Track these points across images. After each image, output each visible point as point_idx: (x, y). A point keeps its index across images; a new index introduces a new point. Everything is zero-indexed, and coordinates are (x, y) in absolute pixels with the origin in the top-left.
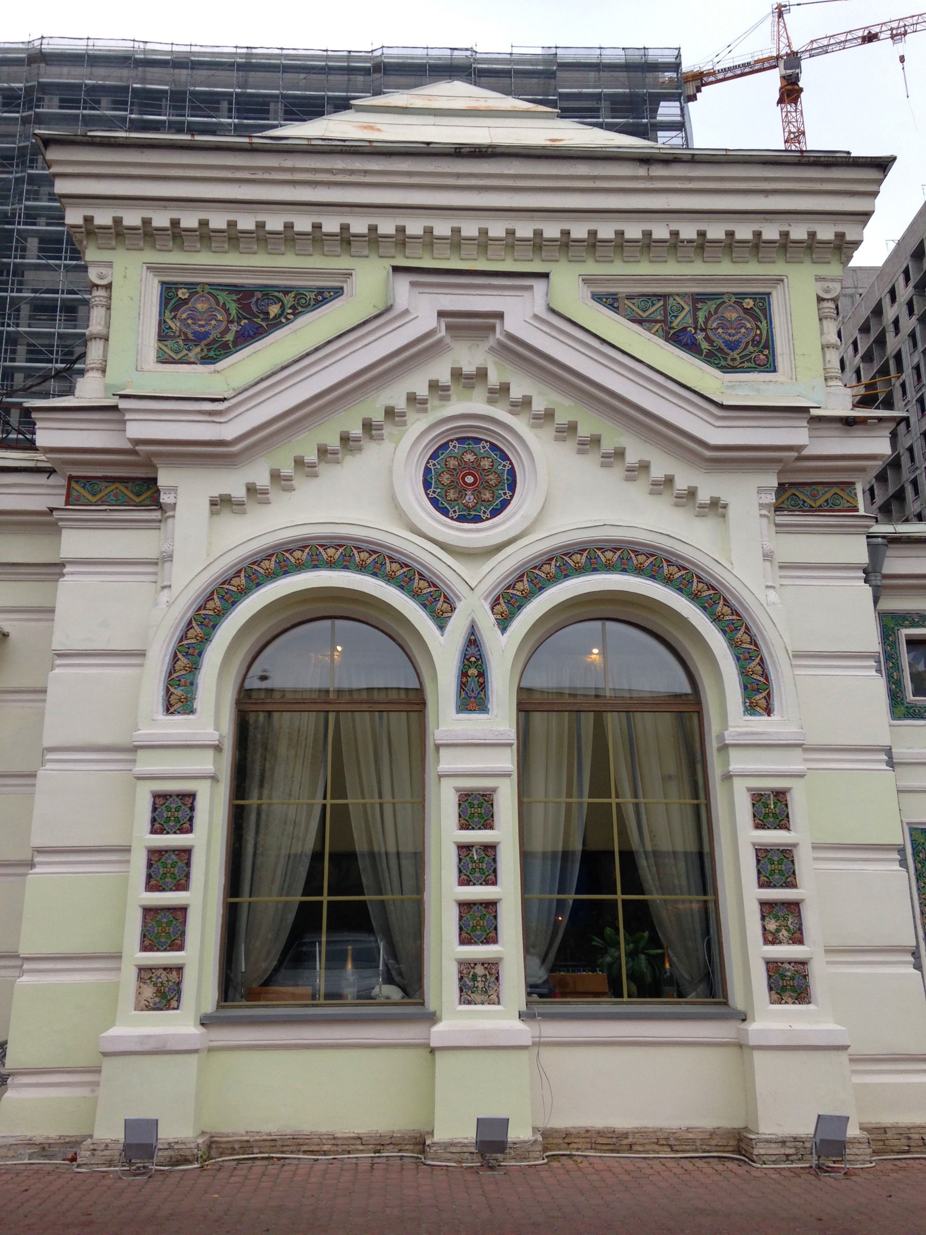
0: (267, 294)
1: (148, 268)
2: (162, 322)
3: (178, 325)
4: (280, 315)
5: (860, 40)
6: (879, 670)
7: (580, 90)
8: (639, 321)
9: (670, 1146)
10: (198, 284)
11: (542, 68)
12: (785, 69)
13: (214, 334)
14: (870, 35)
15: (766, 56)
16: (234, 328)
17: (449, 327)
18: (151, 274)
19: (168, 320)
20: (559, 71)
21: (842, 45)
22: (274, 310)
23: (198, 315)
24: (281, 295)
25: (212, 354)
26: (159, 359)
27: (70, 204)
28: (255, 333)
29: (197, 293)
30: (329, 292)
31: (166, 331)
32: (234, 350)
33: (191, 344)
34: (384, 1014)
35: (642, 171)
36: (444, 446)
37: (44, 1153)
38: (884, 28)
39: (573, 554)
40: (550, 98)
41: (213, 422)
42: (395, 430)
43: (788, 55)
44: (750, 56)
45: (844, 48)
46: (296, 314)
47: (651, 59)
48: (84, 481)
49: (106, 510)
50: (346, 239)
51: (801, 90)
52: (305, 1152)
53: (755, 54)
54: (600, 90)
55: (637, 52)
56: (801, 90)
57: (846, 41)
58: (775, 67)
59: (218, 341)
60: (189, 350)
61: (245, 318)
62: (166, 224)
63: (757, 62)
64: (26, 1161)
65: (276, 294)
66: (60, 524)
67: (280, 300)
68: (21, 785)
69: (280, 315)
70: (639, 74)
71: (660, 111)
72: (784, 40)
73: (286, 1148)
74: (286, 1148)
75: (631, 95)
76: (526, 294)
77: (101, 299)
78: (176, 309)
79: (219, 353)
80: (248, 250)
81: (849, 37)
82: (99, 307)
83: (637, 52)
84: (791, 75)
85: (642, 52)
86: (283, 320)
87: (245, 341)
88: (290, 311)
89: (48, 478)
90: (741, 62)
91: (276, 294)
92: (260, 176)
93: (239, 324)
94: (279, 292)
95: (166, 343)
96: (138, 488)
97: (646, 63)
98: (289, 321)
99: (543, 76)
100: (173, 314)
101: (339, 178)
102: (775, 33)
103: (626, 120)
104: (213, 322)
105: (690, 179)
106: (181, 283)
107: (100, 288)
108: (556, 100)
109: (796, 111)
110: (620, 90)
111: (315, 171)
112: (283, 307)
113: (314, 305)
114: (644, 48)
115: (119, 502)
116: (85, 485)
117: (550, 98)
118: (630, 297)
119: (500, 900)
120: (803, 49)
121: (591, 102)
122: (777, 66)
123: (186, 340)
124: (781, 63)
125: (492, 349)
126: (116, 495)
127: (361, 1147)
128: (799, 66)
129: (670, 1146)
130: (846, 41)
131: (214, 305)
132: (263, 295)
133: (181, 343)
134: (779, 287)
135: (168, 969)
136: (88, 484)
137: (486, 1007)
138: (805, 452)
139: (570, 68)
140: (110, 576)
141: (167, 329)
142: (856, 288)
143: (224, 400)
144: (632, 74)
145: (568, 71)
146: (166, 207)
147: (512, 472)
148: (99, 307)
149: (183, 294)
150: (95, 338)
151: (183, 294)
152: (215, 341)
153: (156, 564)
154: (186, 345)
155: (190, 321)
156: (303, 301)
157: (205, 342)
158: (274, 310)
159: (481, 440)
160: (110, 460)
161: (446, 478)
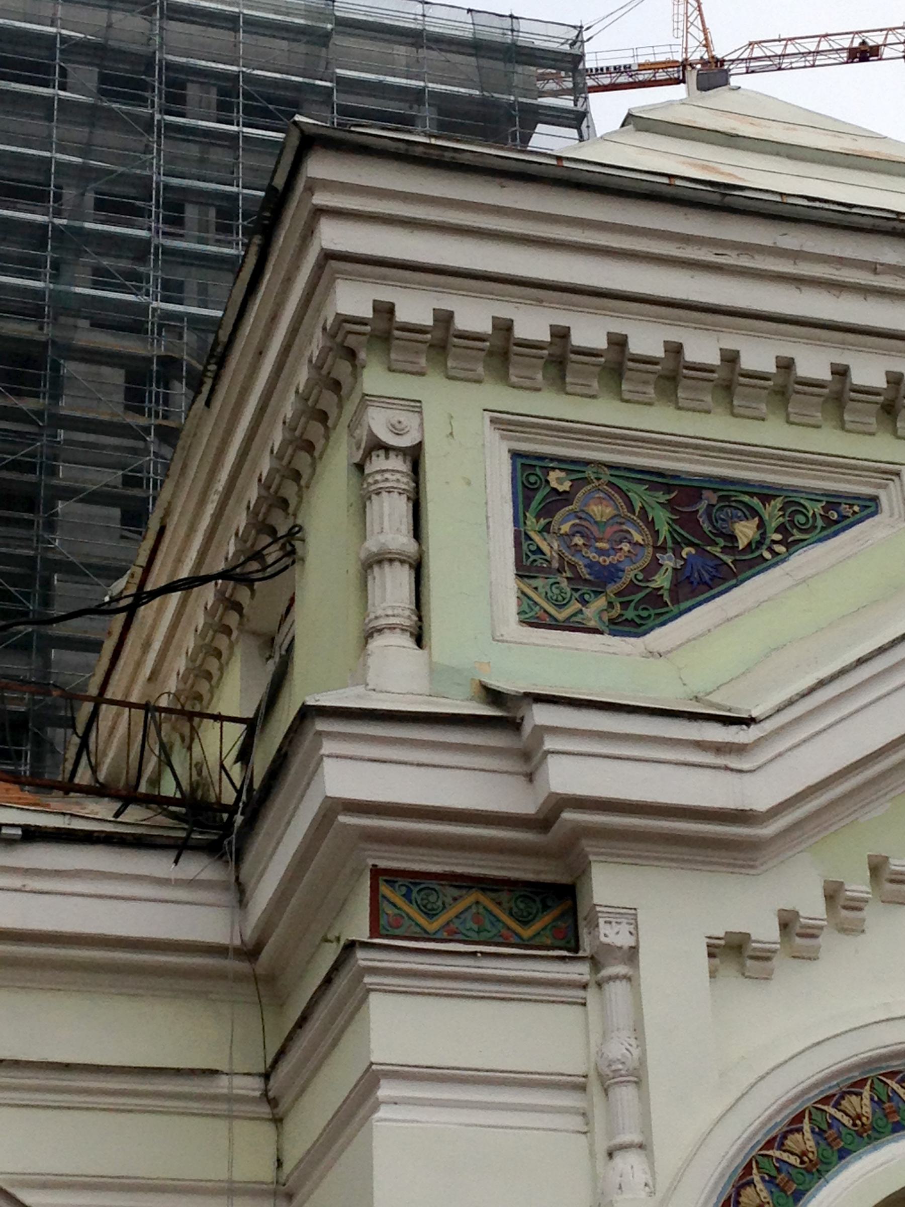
0: (729, 497)
1: (492, 421)
2: (521, 538)
3: (555, 545)
4: (760, 544)
5: (845, 55)
7: (381, 78)
10: (587, 463)
11: (302, 21)
13: (631, 572)
14: (863, 48)
15: (661, 58)
16: (669, 562)
18: (497, 434)
19: (532, 534)
20: (338, 33)
21: (810, 58)
22: (745, 531)
23: (594, 529)
24: (755, 502)
25: (630, 614)
26: (523, 617)
28: (713, 578)
29: (586, 481)
30: (851, 506)
31: (533, 557)
32: (675, 610)
33: (585, 589)
38: (891, 39)
39: (842, 1098)
40: (318, 82)
41: (727, 768)
43: (703, 62)
44: (630, 53)
45: (813, 66)
46: (792, 546)
47: (523, 40)
48: (407, 881)
49: (474, 954)
53: (640, 52)
54: (422, 84)
55: (496, 22)
57: (818, 52)
58: (677, 81)
59: (641, 588)
60: (585, 603)
62: (484, 326)
63: (643, 67)
65: (746, 499)
66: (367, 980)
67: (754, 513)
69: (760, 544)
70: (500, 65)
75: (484, 102)
77: (398, 476)
78: (547, 511)
79: (645, 614)
80: (692, 405)
81: (824, 46)
82: (395, 495)
83: (496, 22)
85: (507, 23)
86: (767, 555)
87: (694, 593)
88: (778, 537)
89: (176, 862)
90: (612, 63)
91: (746, 499)
92: (732, 259)
93: (677, 555)
95: (535, 583)
96: (522, 906)
97: (514, 44)
98: (778, 559)
99: (305, 39)
100: (543, 522)
102: (681, 18)
104: (626, 547)
106: (554, 458)
107: (392, 454)
108: (332, 89)
110: (463, 90)
111: (841, 262)
112: (761, 525)
113: (823, 529)
114: (511, 16)
115: (484, 936)
116: (409, 891)
117: (318, 82)
121: (402, 104)
122: (684, 81)
123: (576, 579)
124: (692, 76)
126: (477, 918)
130: (818, 52)
131: (625, 511)
132: (721, 498)
133: (564, 584)
136: (415, 890)
139: (348, 30)
140: (482, 1113)
141: (533, 552)
143: (749, 721)
144: (485, 63)
145: (354, 35)
146: (541, 301)
148: (395, 495)
149: (558, 480)
150: (391, 561)
151: (559, 481)
152: (633, 587)
153: (582, 1088)
154: (577, 590)
155: (578, 540)
156: (802, 519)
157: (612, 588)
160: (491, 839)
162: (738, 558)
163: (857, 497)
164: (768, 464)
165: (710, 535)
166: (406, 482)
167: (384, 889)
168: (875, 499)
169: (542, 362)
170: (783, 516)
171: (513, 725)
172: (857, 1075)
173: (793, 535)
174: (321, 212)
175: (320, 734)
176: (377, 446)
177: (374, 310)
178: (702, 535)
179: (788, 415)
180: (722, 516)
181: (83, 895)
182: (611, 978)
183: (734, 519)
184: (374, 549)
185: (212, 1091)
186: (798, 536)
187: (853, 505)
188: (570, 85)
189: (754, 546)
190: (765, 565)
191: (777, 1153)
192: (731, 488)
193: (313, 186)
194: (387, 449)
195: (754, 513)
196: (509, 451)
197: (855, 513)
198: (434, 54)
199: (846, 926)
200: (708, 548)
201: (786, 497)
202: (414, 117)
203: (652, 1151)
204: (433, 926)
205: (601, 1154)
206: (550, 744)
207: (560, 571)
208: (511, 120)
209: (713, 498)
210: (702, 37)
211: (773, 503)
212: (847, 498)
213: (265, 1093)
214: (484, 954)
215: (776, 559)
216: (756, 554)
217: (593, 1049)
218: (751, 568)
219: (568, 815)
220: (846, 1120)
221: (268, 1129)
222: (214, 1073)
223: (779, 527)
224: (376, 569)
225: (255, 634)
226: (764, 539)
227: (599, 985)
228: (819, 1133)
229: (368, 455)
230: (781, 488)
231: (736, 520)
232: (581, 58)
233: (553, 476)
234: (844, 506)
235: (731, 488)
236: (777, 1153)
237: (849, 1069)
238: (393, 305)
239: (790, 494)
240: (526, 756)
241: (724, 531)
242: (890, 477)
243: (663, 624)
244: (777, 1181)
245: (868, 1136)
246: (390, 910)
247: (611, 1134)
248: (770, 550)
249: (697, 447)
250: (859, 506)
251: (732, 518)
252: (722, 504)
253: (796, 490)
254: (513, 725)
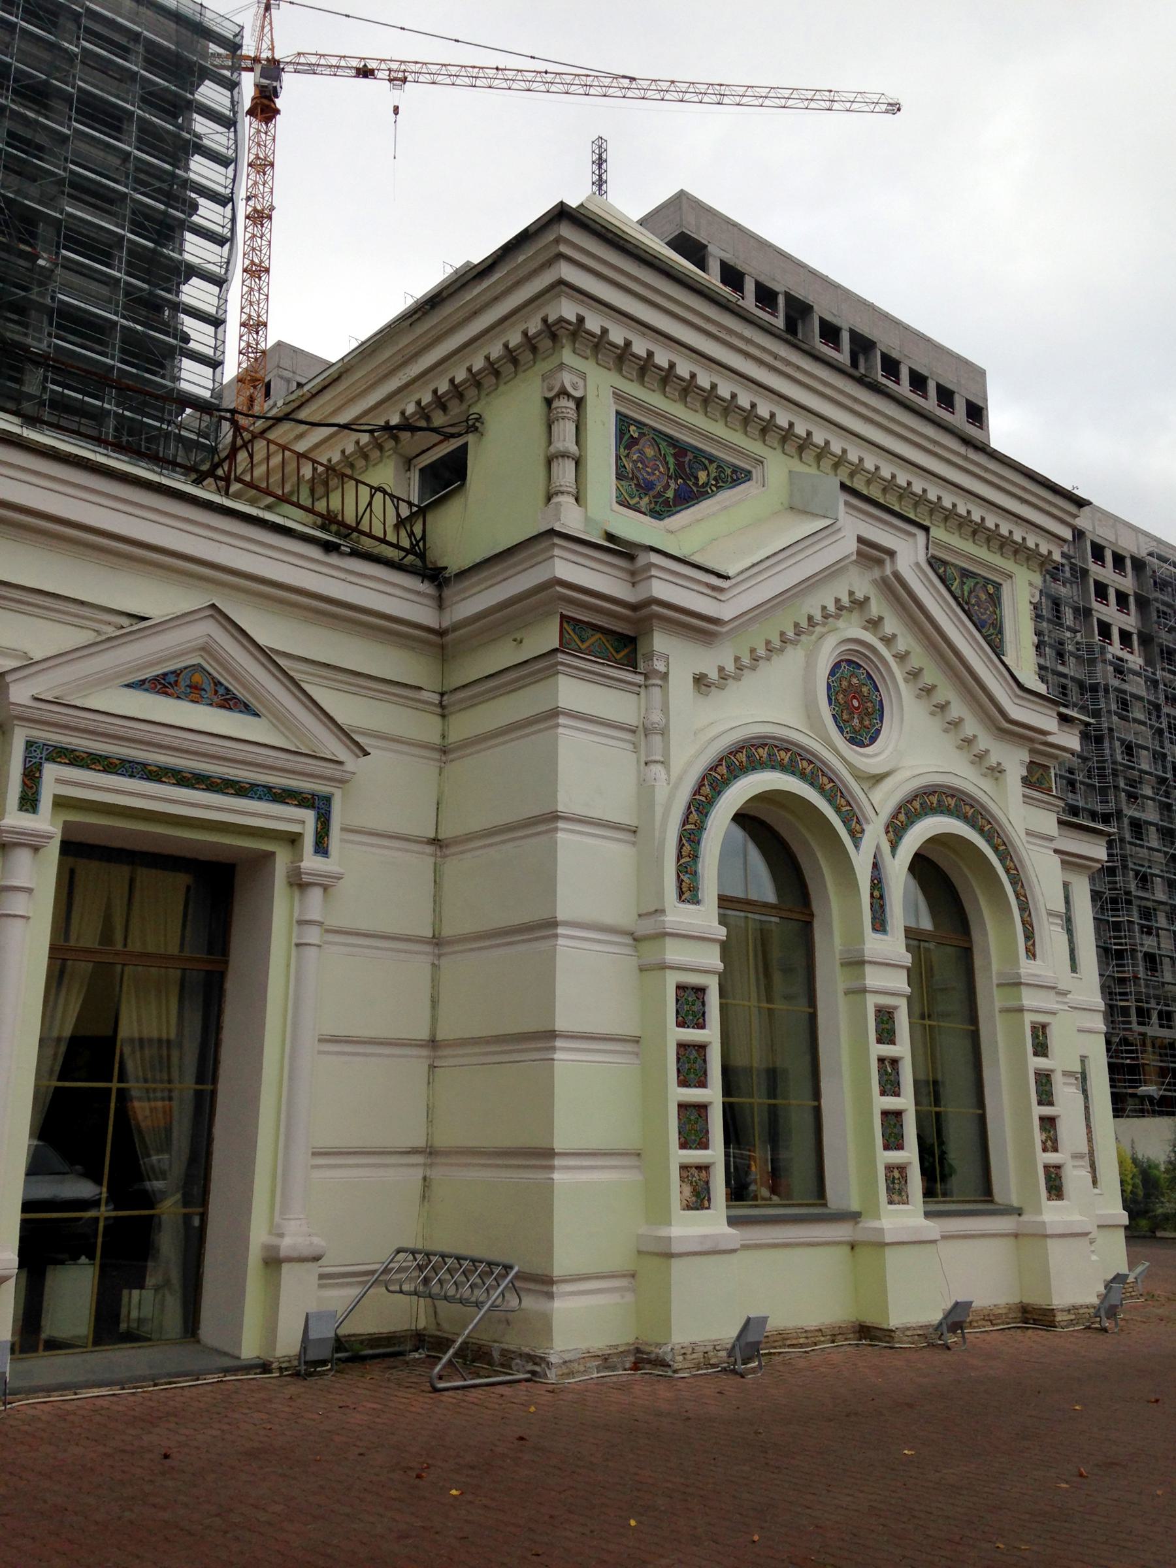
4: (707, 484)
6: (1063, 929)
9: (991, 1321)
10: (646, 425)
12: (262, 76)
13: (659, 488)
16: (673, 485)
17: (859, 553)
22: (702, 476)
24: (707, 462)
27: (567, 294)
33: (641, 491)
34: (763, 1216)
35: (962, 449)
37: (606, 1365)
41: (716, 598)
43: (268, 60)
50: (767, 428)
51: (277, 112)
52: (790, 1346)
56: (277, 112)
61: (682, 478)
64: (596, 1375)
65: (703, 460)
66: (559, 667)
68: (368, 947)
71: (202, 89)
72: (267, 40)
73: (776, 1344)
74: (776, 1344)
76: (910, 540)
78: (628, 447)
84: (266, 87)
85: (198, 8)
88: (714, 482)
91: (703, 460)
92: (723, 335)
94: (706, 458)
95: (623, 483)
98: (714, 494)
100: (626, 451)
101: (778, 364)
103: (166, 84)
104: (657, 472)
105: (986, 470)
106: (635, 421)
109: (266, 133)
110: (165, 43)
114: (201, 5)
119: (905, 1110)
120: (288, 60)
124: (258, 68)
125: (874, 581)
127: (823, 1339)
128: (278, 78)
129: (991, 1321)
134: (1009, 581)
135: (699, 1168)
137: (901, 1207)
138: (1050, 739)
142: (294, 373)
143: (727, 578)
150: (568, 457)
153: (634, 732)
157: (652, 493)
159: (861, 666)
166: (575, 416)
167: (565, 625)
168: (750, 472)
171: (631, 558)
172: (741, 744)
174: (561, 256)
175: (554, 544)
176: (564, 393)
178: (686, 474)
181: (371, 589)
182: (654, 685)
183: (698, 469)
184: (562, 449)
185: (417, 697)
186: (721, 484)
188: (230, 64)
193: (559, 240)
194: (569, 395)
195: (706, 469)
198: (149, 13)
202: (129, 49)
203: (669, 765)
204: (583, 646)
205: (643, 763)
206: (654, 572)
207: (632, 479)
208: (192, 73)
210: (269, 43)
213: (441, 702)
214: (608, 665)
217: (642, 716)
219: (655, 608)
220: (737, 763)
221: (438, 719)
222: (420, 688)
224: (560, 459)
225: (401, 455)
227: (646, 687)
229: (558, 395)
232: (240, 47)
233: (632, 428)
240: (633, 573)
243: (669, 516)
246: (567, 636)
247: (647, 756)
249: (690, 429)
254: (631, 558)
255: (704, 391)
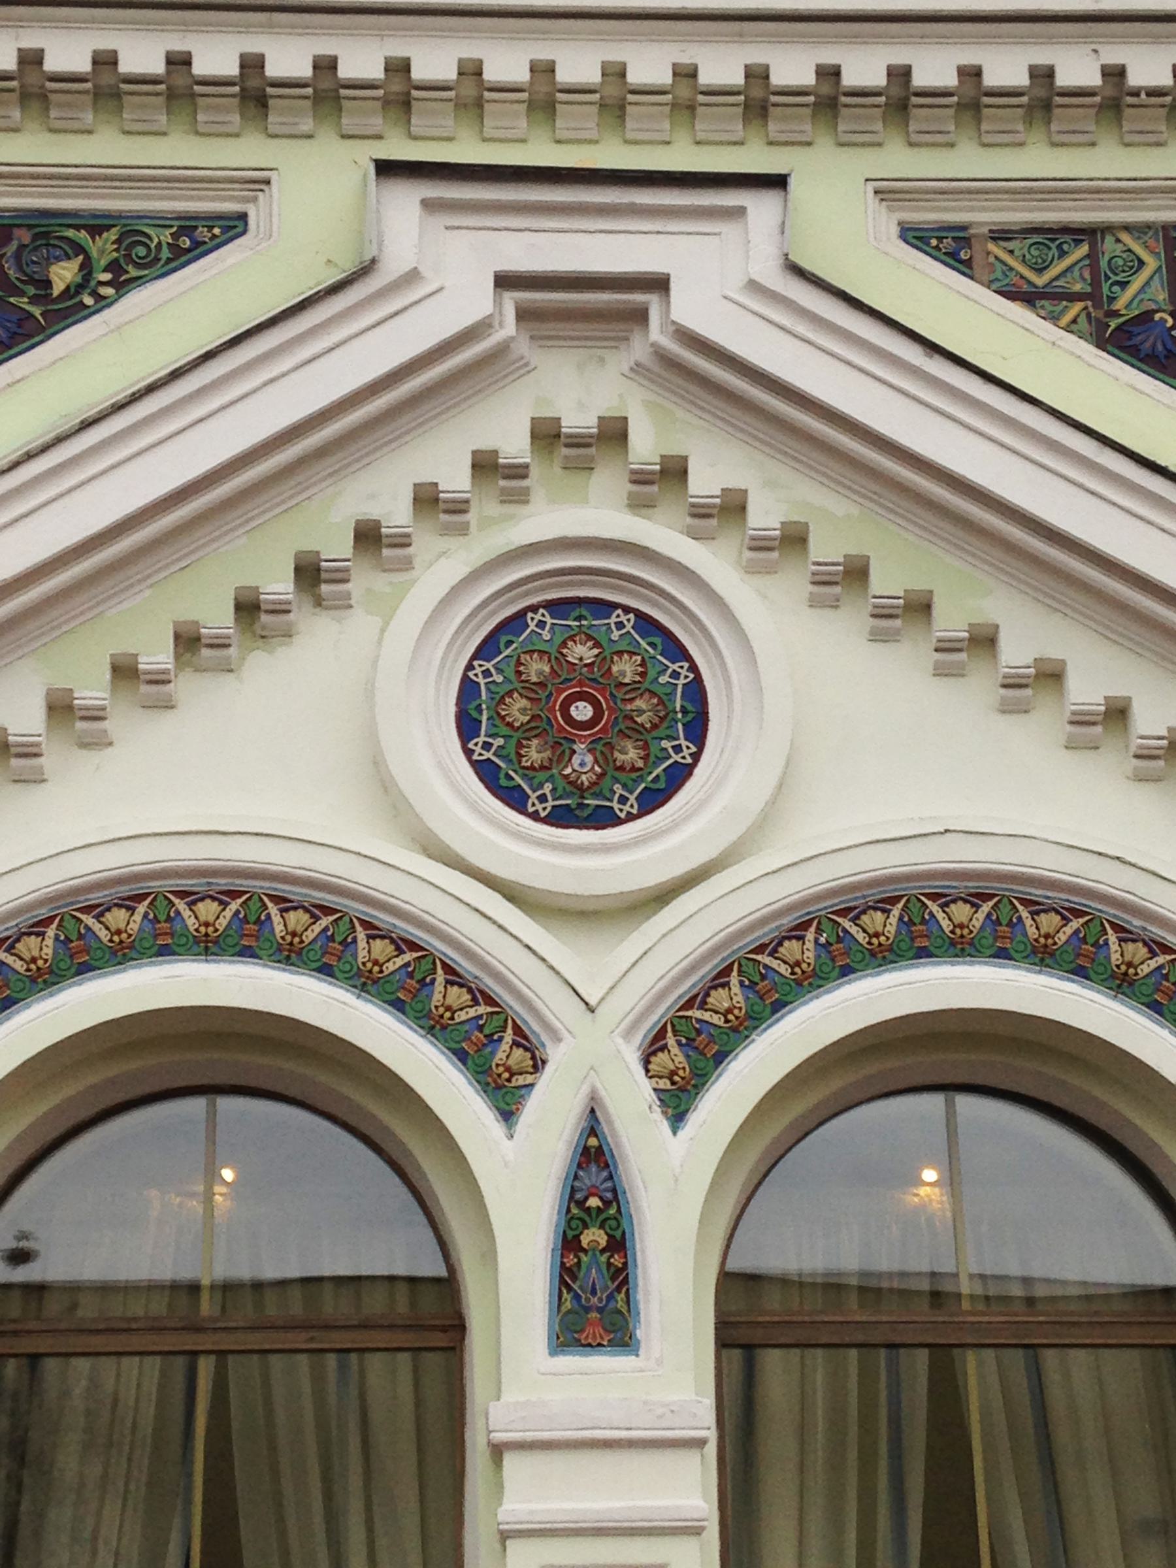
0: (48, 233)
4: (80, 288)
8: (1028, 297)
17: (524, 315)
24: (82, 236)
30: (211, 228)
36: (514, 623)
42: (381, 582)
46: (122, 285)
65: (70, 233)
67: (79, 249)
76: (727, 229)
86: (88, 300)
88: (107, 277)
91: (70, 233)
94: (77, 228)
98: (103, 303)
112: (87, 267)
113: (169, 260)
118: (1001, 235)
125: (638, 369)
132: (36, 237)
147: (697, 691)
158: (63, 274)
161: (518, 709)
162: (49, 307)
163: (220, 217)
164: (188, 189)
165: (18, 284)
169: (1164, 111)
170: (116, 250)
172: (44, 913)
173: (127, 272)
177: (1032, 76)
179: (1122, 138)
180: (34, 259)
183: (49, 261)
186: (133, 272)
187: (213, 227)
189: (72, 290)
190: (86, 312)
191: (698, 1014)
192: (53, 221)
196: (899, 224)
197: (214, 236)
199: (86, 740)
200: (12, 300)
201: (125, 225)
209: (25, 236)
211: (105, 235)
212: (204, 219)
215: (99, 306)
216: (77, 300)
218: (66, 318)
220: (784, 969)
223: (110, 264)
226: (88, 281)
228: (750, 986)
230: (119, 216)
231: (52, 260)
234: (200, 229)
235: (53, 221)
236: (698, 1014)
237: (30, 907)
238: (624, 65)
239: (129, 222)
241: (36, 277)
242: (257, 186)
244: (696, 1044)
245: (45, 981)
248: (94, 294)
250: (220, 227)
251: (48, 259)
252: (39, 243)
253: (140, 216)
255: (1021, 94)
